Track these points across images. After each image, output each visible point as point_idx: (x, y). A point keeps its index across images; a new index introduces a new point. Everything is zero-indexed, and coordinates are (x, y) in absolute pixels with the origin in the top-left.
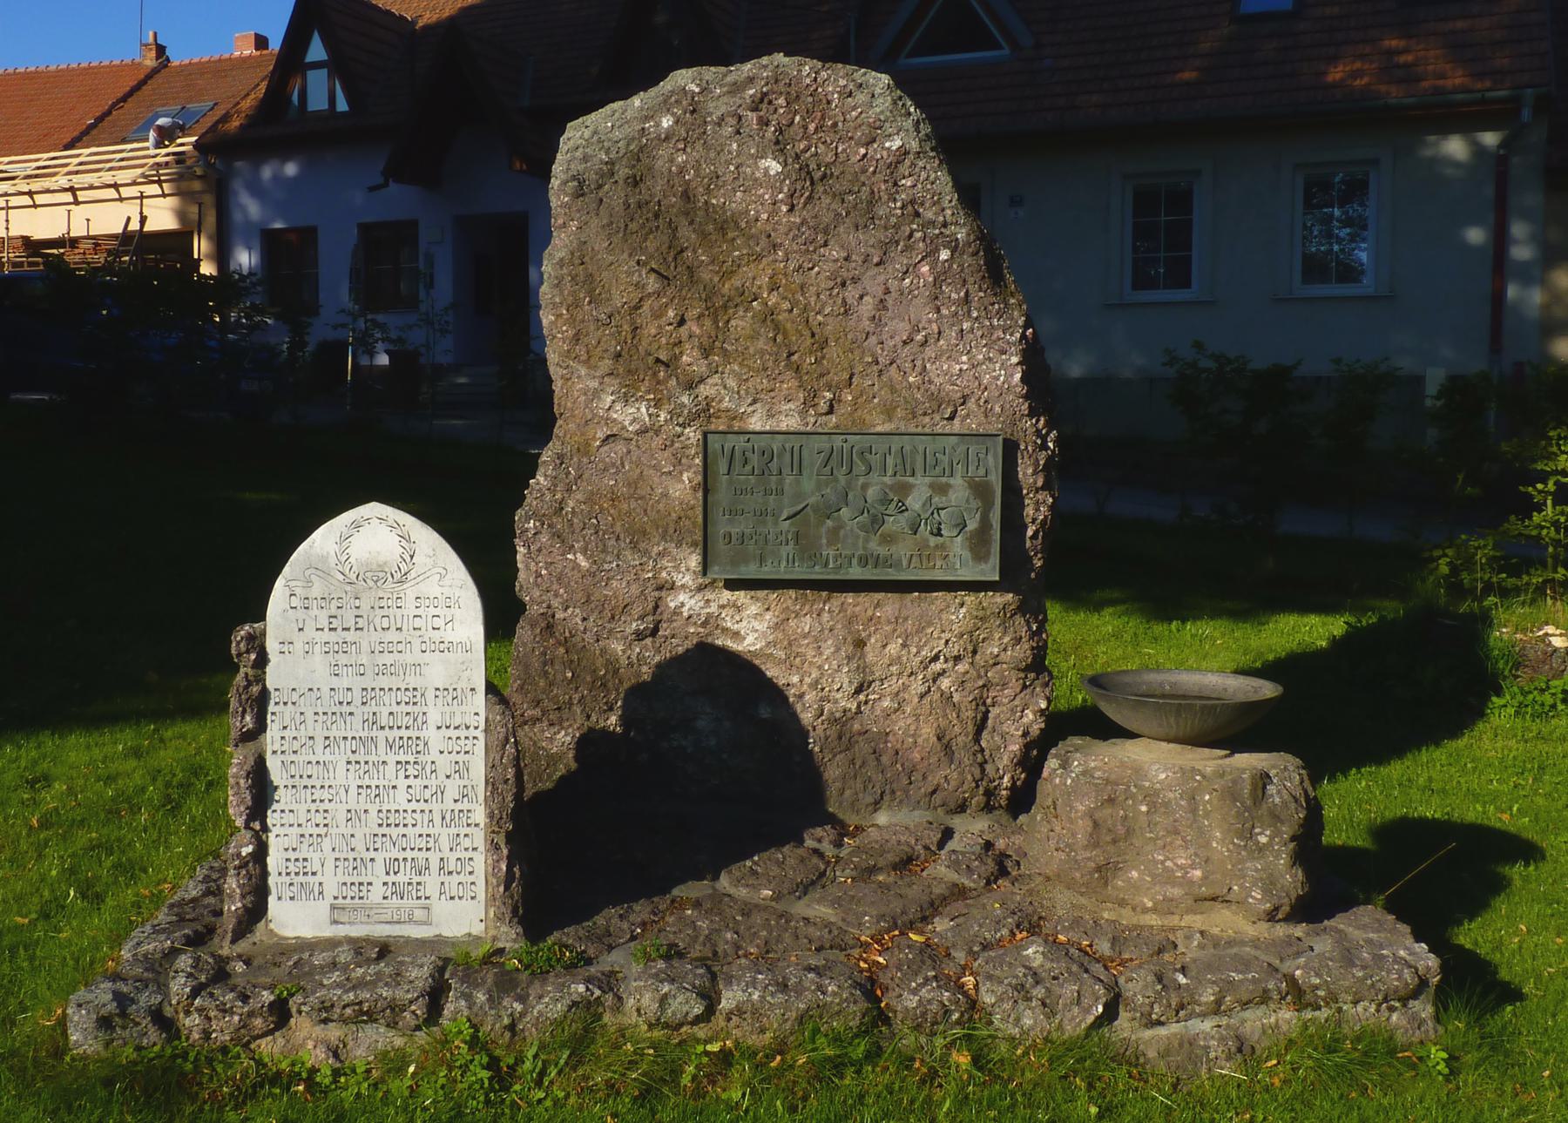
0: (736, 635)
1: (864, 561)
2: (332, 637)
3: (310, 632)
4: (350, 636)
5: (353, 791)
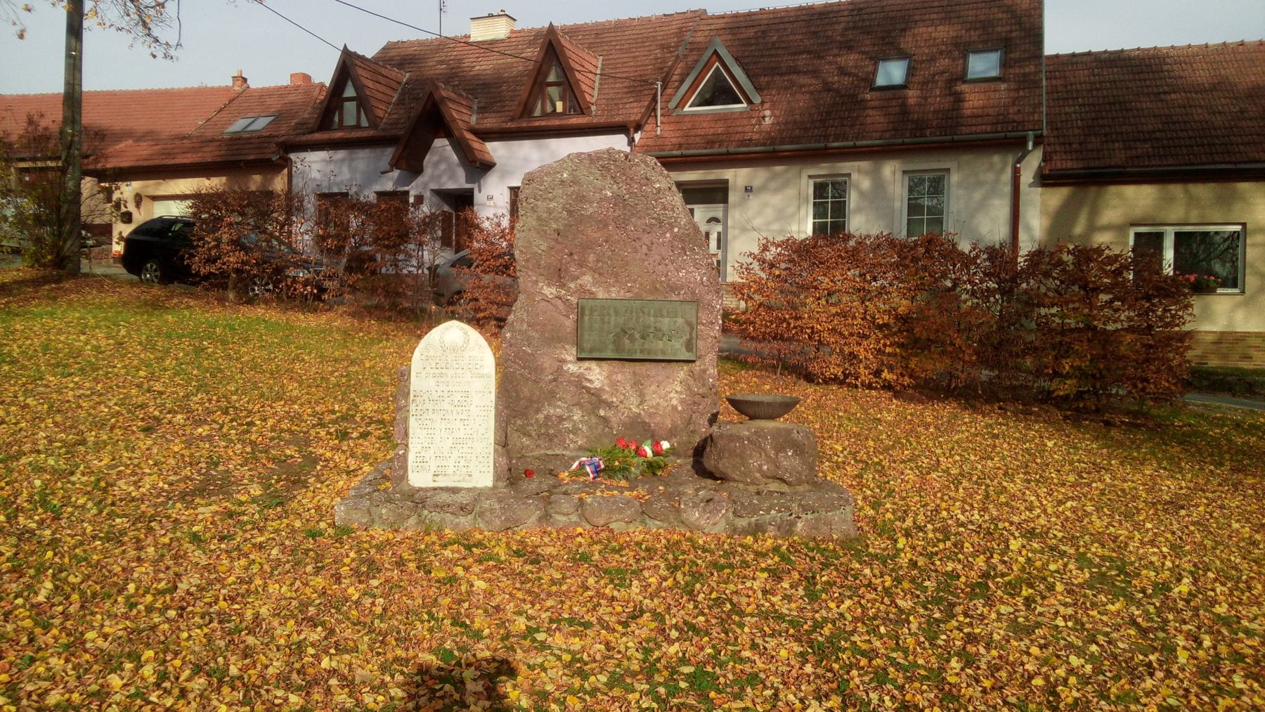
0: (590, 381)
1: (642, 351)
2: (437, 371)
3: (428, 368)
4: (444, 371)
5: (443, 430)
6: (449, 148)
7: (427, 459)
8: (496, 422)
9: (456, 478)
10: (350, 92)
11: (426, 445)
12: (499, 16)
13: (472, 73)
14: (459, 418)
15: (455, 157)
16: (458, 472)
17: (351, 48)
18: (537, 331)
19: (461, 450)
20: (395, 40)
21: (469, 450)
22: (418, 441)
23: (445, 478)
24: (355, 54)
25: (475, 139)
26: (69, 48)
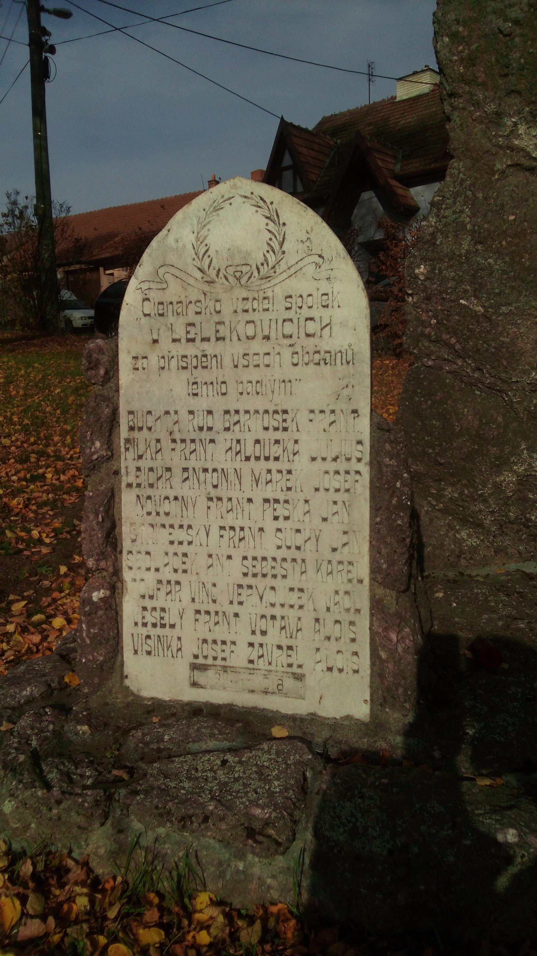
2: (191, 350)
3: (165, 344)
4: (210, 348)
5: (215, 532)
6: (375, 199)
7: (172, 617)
8: (375, 509)
9: (258, 681)
10: (287, 161)
11: (167, 574)
12: (423, 71)
13: (397, 128)
14: (258, 495)
15: (381, 208)
16: (261, 664)
17: (286, 119)
18: (498, 252)
19: (269, 596)
20: (328, 114)
21: (293, 599)
22: (147, 562)
23: (226, 678)
24: (291, 125)
25: (400, 186)
26: (35, 130)
